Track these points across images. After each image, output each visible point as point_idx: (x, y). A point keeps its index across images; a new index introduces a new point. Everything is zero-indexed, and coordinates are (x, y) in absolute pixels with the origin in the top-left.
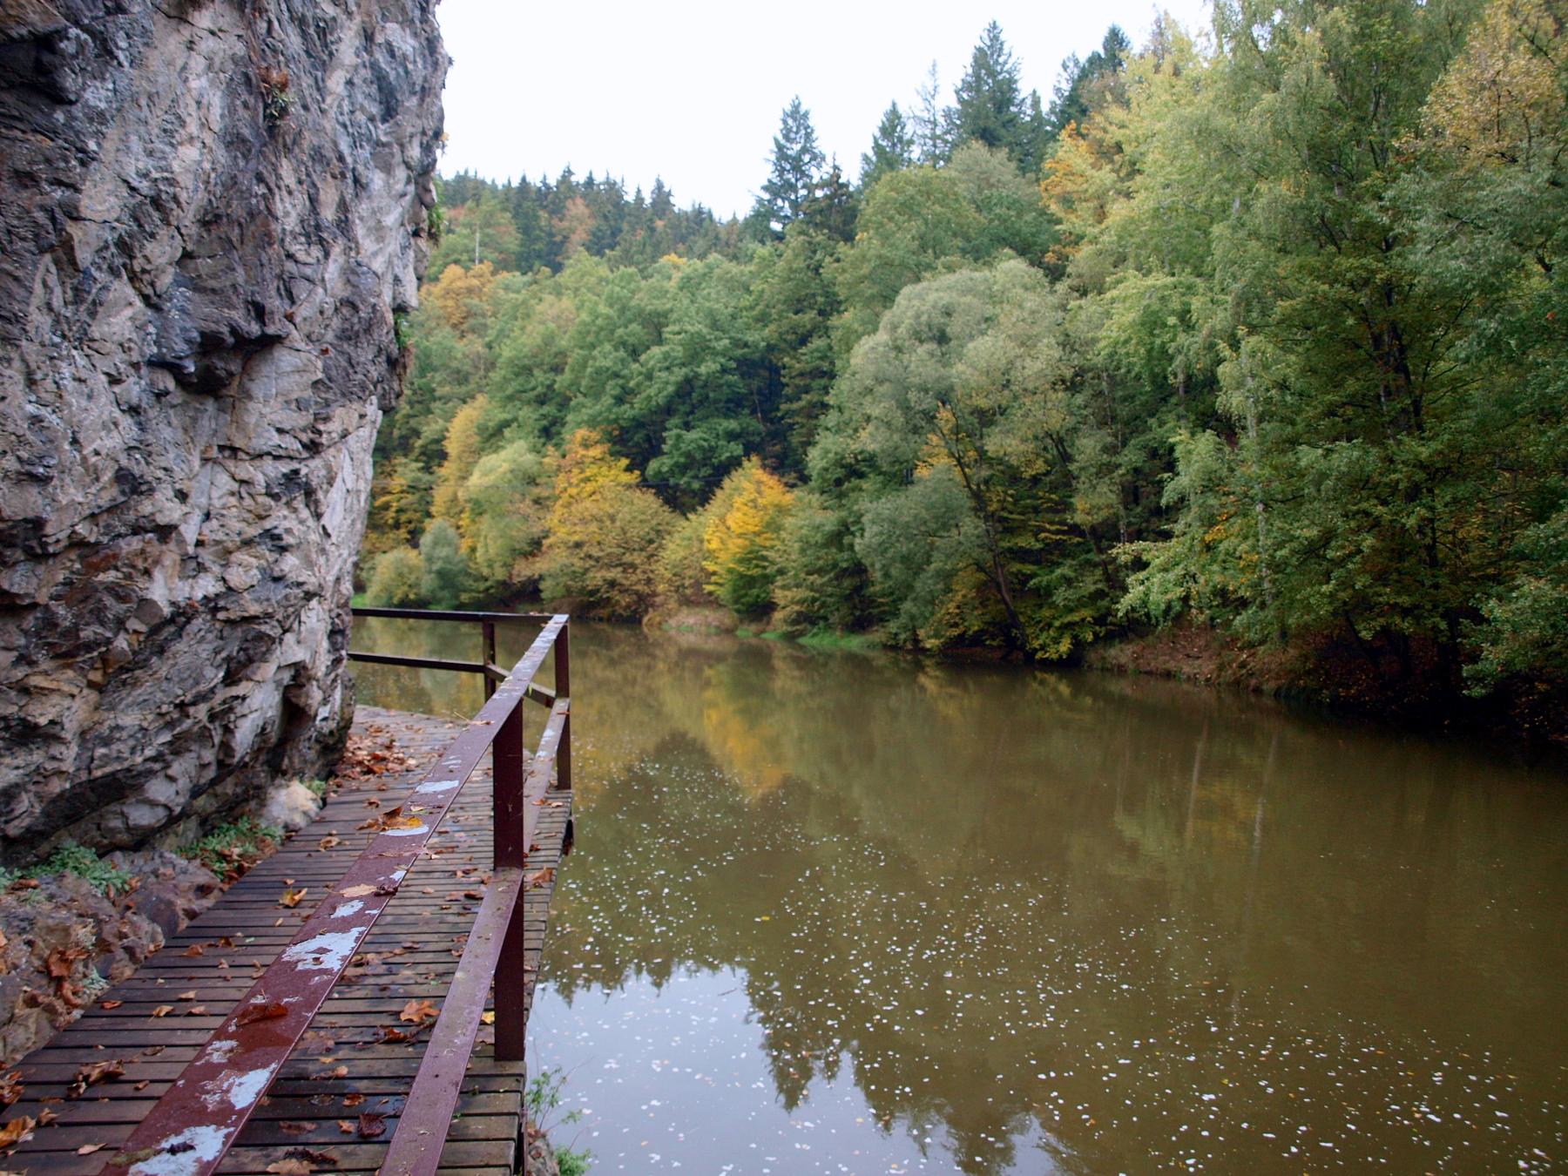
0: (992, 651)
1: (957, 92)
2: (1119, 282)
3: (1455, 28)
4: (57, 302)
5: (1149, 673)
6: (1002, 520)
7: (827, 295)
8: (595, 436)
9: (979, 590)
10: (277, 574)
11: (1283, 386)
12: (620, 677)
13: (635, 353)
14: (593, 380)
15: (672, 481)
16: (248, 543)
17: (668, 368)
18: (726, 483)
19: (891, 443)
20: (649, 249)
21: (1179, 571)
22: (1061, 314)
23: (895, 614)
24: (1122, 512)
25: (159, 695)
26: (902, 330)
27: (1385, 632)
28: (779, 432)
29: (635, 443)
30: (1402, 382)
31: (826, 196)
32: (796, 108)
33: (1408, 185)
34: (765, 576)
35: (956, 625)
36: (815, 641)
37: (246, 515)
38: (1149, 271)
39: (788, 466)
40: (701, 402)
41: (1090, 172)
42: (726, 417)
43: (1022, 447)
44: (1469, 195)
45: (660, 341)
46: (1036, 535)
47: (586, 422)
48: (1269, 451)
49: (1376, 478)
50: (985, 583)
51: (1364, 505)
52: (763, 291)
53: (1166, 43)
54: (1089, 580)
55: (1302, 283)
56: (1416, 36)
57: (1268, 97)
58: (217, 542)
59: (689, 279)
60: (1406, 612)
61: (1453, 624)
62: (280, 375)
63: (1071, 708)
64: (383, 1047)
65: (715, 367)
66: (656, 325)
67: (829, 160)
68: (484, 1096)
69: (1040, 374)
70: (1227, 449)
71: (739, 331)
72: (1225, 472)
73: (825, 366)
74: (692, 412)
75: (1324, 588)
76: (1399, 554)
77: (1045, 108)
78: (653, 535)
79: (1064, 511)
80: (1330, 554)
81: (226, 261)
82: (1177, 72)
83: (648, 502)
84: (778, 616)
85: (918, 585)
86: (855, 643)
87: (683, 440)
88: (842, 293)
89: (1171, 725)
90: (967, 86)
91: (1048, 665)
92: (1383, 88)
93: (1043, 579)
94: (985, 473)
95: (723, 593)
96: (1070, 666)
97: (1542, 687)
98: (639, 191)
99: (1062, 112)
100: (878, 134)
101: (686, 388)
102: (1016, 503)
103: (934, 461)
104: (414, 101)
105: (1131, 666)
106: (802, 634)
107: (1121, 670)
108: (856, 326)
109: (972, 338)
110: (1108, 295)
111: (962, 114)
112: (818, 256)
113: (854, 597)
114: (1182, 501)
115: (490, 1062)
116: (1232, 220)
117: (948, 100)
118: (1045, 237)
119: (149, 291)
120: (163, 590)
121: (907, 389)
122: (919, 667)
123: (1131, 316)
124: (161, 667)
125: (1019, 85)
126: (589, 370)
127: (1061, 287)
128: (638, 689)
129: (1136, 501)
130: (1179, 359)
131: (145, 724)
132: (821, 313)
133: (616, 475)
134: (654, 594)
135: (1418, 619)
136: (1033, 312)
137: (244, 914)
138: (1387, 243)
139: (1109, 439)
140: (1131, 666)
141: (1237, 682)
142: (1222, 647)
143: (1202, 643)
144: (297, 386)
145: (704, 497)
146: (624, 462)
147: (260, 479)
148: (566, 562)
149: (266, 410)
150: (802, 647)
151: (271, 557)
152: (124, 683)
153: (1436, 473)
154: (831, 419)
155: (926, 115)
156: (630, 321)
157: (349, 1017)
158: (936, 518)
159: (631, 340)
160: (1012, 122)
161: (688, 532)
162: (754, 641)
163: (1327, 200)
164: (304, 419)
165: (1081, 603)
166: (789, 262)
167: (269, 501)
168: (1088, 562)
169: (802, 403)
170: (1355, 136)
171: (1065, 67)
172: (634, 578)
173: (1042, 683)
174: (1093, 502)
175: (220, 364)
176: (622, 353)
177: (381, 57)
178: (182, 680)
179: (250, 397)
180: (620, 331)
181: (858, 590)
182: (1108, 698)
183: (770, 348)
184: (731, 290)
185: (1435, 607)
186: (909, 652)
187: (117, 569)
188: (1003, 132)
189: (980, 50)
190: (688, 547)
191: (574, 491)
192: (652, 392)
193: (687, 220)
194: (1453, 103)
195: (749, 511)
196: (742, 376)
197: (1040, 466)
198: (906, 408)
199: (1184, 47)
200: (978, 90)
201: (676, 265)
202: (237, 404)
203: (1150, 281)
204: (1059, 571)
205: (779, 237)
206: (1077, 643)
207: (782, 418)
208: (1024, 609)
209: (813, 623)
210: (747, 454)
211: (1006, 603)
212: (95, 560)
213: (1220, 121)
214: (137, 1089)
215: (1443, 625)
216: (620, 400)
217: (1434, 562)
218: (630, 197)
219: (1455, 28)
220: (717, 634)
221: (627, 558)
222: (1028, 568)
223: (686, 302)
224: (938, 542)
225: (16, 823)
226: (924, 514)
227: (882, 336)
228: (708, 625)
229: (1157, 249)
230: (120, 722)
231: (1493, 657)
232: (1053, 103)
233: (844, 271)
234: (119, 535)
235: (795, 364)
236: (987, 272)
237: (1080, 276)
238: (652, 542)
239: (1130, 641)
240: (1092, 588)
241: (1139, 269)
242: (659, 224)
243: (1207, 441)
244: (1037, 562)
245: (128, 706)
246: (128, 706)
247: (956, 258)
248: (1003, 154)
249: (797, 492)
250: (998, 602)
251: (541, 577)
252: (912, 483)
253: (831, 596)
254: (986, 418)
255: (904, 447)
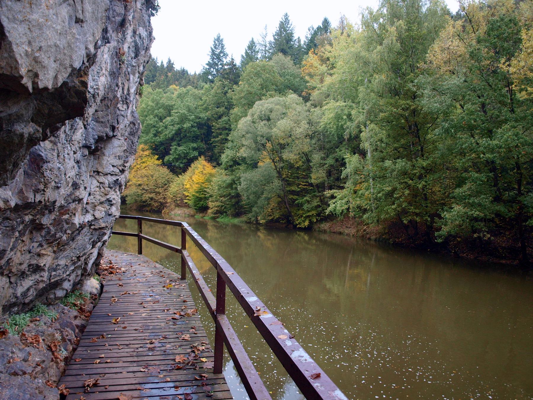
0: (283, 224)
1: (273, 36)
2: (327, 103)
3: (436, 30)
4: (67, 130)
5: (334, 233)
6: (287, 181)
7: (228, 102)
8: (146, 147)
9: (278, 204)
10: (110, 213)
11: (381, 141)
12: (154, 232)
13: (161, 119)
14: (146, 128)
15: (173, 164)
16: (101, 203)
17: (172, 125)
18: (192, 165)
19: (251, 154)
20: (166, 83)
21: (346, 200)
22: (308, 113)
23: (250, 211)
24: (326, 179)
25: (72, 254)
26: (256, 117)
27: (410, 221)
28: (211, 148)
29: (160, 150)
30: (417, 140)
31: (229, 69)
32: (219, 38)
33: (422, 79)
34: (205, 198)
35: (271, 215)
36: (222, 220)
37: (102, 194)
38: (337, 101)
39: (214, 160)
40: (184, 137)
41: (319, 67)
42: (192, 142)
43: (295, 157)
44: (440, 83)
45: (170, 115)
46: (298, 186)
47: (144, 142)
48: (375, 161)
49: (409, 171)
50: (280, 202)
51: (406, 180)
52: (206, 100)
53: (343, 26)
54: (315, 201)
55: (387, 108)
56: (425, 31)
57: (379, 47)
58: (93, 203)
59: (181, 94)
60: (417, 215)
61: (432, 219)
62: (114, 147)
63: (308, 243)
64: (176, 371)
65: (189, 125)
66: (169, 110)
67: (230, 56)
68: (217, 385)
69: (301, 133)
70: (362, 160)
71: (198, 113)
72: (362, 168)
73: (227, 126)
74: (181, 140)
75: (393, 207)
76: (415, 196)
77: (302, 43)
78: (166, 182)
79: (307, 178)
80: (395, 196)
81: (106, 112)
82: (349, 36)
83: (165, 171)
84: (210, 211)
85: (259, 202)
86: (236, 221)
87: (178, 150)
88: (235, 102)
89: (341, 249)
90: (277, 34)
91: (301, 229)
92: (414, 47)
93: (300, 201)
94: (282, 165)
95: (190, 203)
96: (308, 230)
97: (459, 239)
98: (162, 62)
99: (308, 45)
100: (247, 49)
101: (178, 133)
102: (291, 176)
103: (265, 160)
104: (144, 52)
105: (328, 230)
106: (218, 217)
107: (325, 232)
108: (239, 114)
109: (279, 120)
110: (324, 108)
111: (275, 43)
112: (226, 89)
113: (235, 205)
114: (347, 178)
115: (212, 375)
116: (365, 86)
117: (270, 38)
118: (302, 87)
119: (86, 123)
120: (77, 220)
121: (257, 136)
122: (258, 230)
123: (332, 115)
124: (73, 245)
125: (294, 35)
126: (145, 124)
127: (308, 104)
128: (160, 235)
129: (330, 175)
130: (348, 131)
131: (67, 264)
132: (226, 108)
133: (153, 161)
134: (166, 203)
135: (422, 217)
136: (299, 112)
137: (101, 327)
138: (414, 97)
139: (323, 155)
140: (328, 230)
141: (363, 236)
142: (358, 224)
143: (351, 223)
144: (119, 151)
145: (184, 170)
146: (157, 157)
147: (107, 182)
148: (136, 191)
149: (109, 159)
150: (218, 222)
151: (108, 207)
152: (61, 250)
153: (428, 170)
154: (229, 144)
155: (263, 43)
156: (160, 108)
157: (159, 361)
158: (265, 179)
159: (160, 115)
160: (291, 47)
161: (179, 182)
162: (201, 220)
163: (397, 81)
164: (120, 162)
165: (312, 209)
166: (216, 90)
167: (109, 189)
168: (315, 195)
169: (219, 139)
170: (405, 62)
171: (309, 30)
172: (159, 197)
173: (299, 235)
174: (317, 176)
175: (100, 145)
176: (156, 119)
177: (137, 38)
178: (79, 249)
179: (104, 155)
180: (156, 111)
181: (237, 203)
182: (320, 240)
183: (208, 119)
184: (195, 99)
185: (426, 213)
186: (254, 224)
187: (68, 214)
188: (289, 50)
189: (282, 22)
190: (178, 187)
191: (139, 166)
192: (167, 133)
193: (179, 73)
194: (436, 54)
195: (200, 175)
196: (198, 129)
197: (300, 163)
198: (256, 142)
199: (350, 27)
200: (281, 36)
201: (175, 89)
202: (100, 157)
203: (338, 104)
204: (305, 198)
205: (212, 81)
206: (311, 222)
207: (212, 143)
208: (294, 211)
209: (222, 214)
210: (200, 155)
211: (290, 208)
212: (62, 211)
213: (363, 54)
214: (106, 388)
215: (429, 219)
216: (155, 135)
217: (426, 199)
218: (159, 64)
219: (436, 30)
220: (188, 217)
221: (157, 190)
222: (295, 197)
223: (179, 102)
224: (266, 188)
225: (28, 298)
226: (262, 179)
227: (249, 118)
228: (185, 214)
229: (340, 93)
230: (59, 263)
231: (445, 230)
232: (305, 41)
233: (235, 95)
234: (70, 203)
235: (216, 125)
236: (284, 98)
237: (314, 100)
238: (166, 185)
239: (328, 222)
240: (316, 204)
241: (334, 99)
242: (169, 74)
243: (356, 158)
244: (298, 195)
245: (62, 258)
246: (62, 258)
247: (273, 92)
248: (289, 58)
249: (217, 169)
250: (285, 208)
251: (126, 196)
252: (257, 167)
253: (228, 205)
254: (283, 147)
255: (255, 155)
